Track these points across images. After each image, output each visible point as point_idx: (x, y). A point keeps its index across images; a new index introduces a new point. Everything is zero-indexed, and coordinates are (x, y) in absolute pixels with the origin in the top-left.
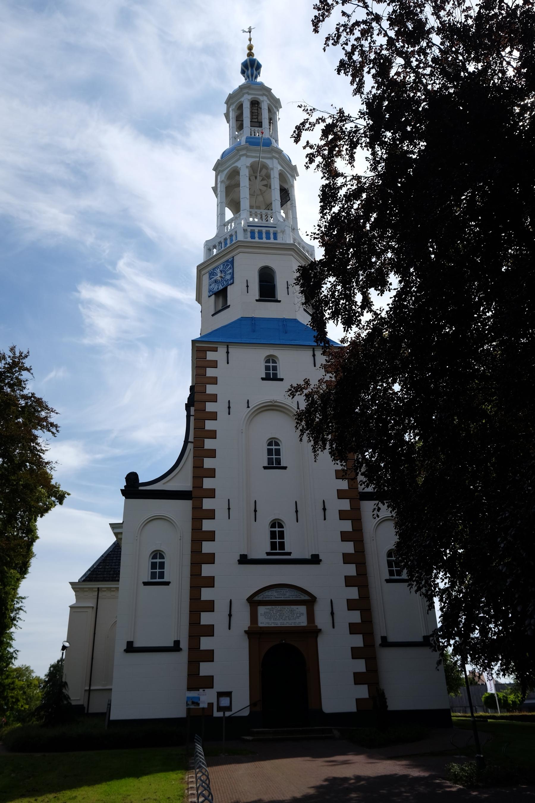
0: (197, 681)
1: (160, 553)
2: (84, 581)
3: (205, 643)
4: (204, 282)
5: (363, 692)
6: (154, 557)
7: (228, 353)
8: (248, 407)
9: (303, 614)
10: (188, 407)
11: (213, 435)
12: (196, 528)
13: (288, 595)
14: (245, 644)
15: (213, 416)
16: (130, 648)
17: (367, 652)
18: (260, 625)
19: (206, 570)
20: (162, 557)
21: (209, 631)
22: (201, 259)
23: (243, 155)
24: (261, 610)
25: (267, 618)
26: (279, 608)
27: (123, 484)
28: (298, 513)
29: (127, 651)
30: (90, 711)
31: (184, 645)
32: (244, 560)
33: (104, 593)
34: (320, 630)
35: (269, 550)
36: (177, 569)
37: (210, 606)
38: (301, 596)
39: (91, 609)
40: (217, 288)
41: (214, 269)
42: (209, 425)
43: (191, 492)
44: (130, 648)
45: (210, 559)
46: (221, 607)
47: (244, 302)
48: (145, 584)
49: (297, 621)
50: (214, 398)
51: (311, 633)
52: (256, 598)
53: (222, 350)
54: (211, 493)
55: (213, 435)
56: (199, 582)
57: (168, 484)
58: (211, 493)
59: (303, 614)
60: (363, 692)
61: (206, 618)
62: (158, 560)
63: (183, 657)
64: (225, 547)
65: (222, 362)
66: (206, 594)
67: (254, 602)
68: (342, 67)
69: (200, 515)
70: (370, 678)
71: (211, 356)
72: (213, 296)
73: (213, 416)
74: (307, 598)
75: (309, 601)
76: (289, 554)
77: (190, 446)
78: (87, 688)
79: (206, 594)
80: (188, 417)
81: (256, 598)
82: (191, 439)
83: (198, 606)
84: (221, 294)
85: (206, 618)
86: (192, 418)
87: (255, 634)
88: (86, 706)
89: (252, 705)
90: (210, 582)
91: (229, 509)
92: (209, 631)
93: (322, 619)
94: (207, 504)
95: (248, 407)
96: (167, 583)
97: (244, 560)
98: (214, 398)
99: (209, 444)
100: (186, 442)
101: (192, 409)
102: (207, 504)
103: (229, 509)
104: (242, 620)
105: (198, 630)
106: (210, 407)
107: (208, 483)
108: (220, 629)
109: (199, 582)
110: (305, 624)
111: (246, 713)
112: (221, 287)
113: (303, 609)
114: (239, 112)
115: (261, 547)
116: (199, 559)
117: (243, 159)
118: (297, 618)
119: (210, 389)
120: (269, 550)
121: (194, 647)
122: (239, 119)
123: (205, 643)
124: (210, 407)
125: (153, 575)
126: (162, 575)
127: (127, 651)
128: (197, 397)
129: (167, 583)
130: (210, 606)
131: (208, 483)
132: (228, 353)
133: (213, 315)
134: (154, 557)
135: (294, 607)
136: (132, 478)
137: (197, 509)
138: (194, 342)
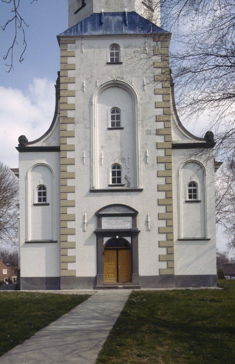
1: (43, 187)
17: (168, 246)
18: (103, 228)
25: (107, 224)
27: (17, 144)
28: (15, 4)
34: (140, 231)
35: (111, 183)
38: (129, 211)
51: (134, 233)
52: (101, 213)
60: (164, 265)
62: (116, 170)
67: (99, 216)
68: (153, 41)
70: (169, 258)
74: (133, 212)
75: (133, 214)
76: (123, 185)
87: (100, 234)
93: (141, 226)
96: (48, 204)
113: (130, 219)
118: (125, 224)
120: (111, 183)
128: (62, 80)
129: (48, 204)
134: (40, 189)
136: (22, 139)
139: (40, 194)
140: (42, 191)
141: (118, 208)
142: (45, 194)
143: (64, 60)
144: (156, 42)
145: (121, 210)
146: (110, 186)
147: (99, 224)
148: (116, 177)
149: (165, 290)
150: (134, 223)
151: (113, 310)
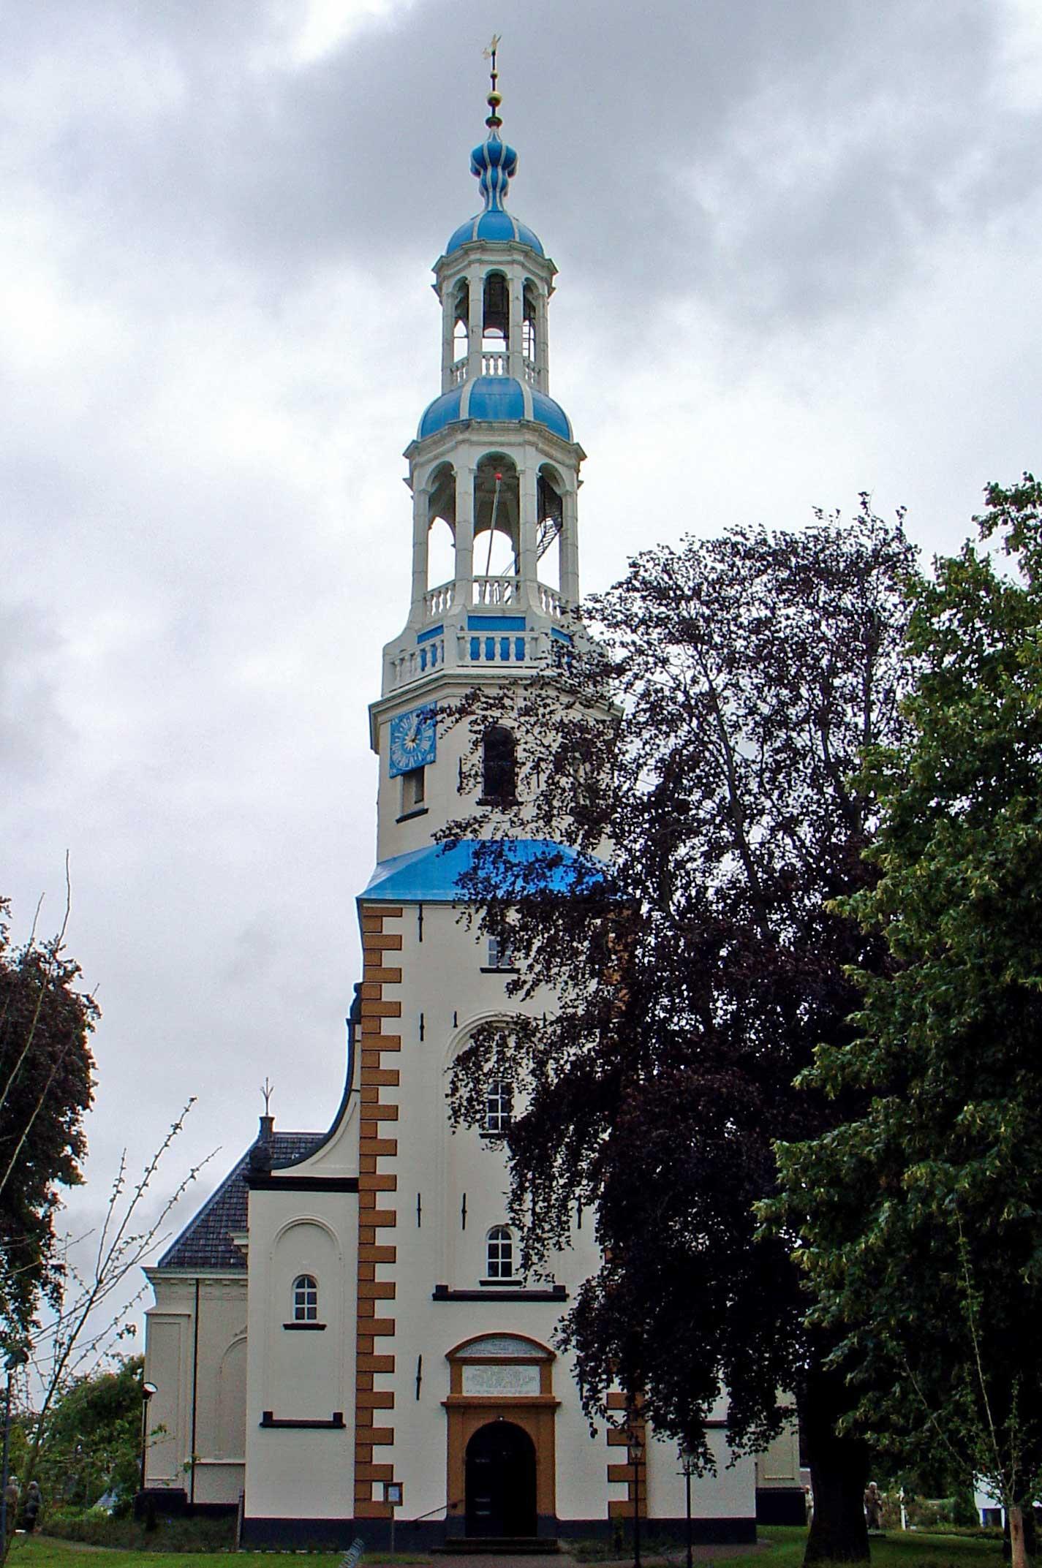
0: (366, 1472)
2: (169, 1263)
3: (381, 1419)
4: (381, 734)
5: (621, 1492)
6: (300, 1285)
7: (421, 919)
8: (456, 1026)
9: (533, 1379)
10: (351, 1023)
11: (393, 1079)
12: (366, 1243)
13: (512, 1350)
14: (442, 1421)
15: (394, 1044)
16: (268, 1421)
19: (382, 1310)
20: (312, 1285)
21: (387, 1401)
22: (362, 872)
23: (463, 441)
24: (468, 1371)
25: (478, 1384)
26: (496, 1368)
29: (263, 1425)
30: (196, 1501)
31: (349, 1420)
32: (442, 1294)
33: (209, 1289)
34: (559, 1404)
36: (337, 1304)
37: (388, 1365)
39: (185, 1319)
40: (408, 763)
41: (401, 719)
42: (387, 1061)
43: (356, 1180)
44: (268, 1421)
45: (389, 1291)
46: (405, 1368)
47: (453, 800)
48: (287, 1327)
49: (525, 1389)
50: (395, 1010)
52: (460, 1355)
53: (411, 914)
54: (390, 1184)
55: (393, 1079)
56: (370, 1328)
57: (320, 1165)
58: (390, 1184)
59: (533, 1379)
60: (621, 1492)
61: (381, 1383)
63: (345, 1440)
64: (409, 1277)
65: (409, 940)
66: (382, 1346)
67: (456, 1360)
69: (371, 1221)
71: (390, 926)
72: (399, 778)
73: (394, 1044)
77: (355, 1098)
78: (188, 1460)
79: (382, 1346)
80: (352, 1042)
81: (458, 1355)
82: (356, 1085)
83: (370, 1365)
84: (415, 775)
85: (381, 1383)
86: (358, 1047)
87: (456, 1408)
88: (188, 1490)
89: (452, 1506)
90: (388, 1328)
91: (419, 1210)
92: (387, 1401)
94: (384, 1201)
95: (456, 1026)
96: (322, 1327)
97: (442, 1294)
98: (395, 1010)
99: (386, 1096)
100: (349, 1090)
101: (358, 1028)
102: (384, 1201)
103: (419, 1210)
104: (438, 1387)
105: (369, 1401)
106: (389, 1027)
107: (384, 1166)
108: (403, 1395)
109: (370, 1328)
110: (537, 1394)
111: (441, 1516)
112: (412, 765)
113: (534, 1371)
114: (460, 295)
115: (473, 1273)
116: (370, 1291)
117: (464, 449)
119: (389, 993)
121: (364, 1424)
122: (461, 311)
123: (381, 1419)
124: (389, 1027)
125: (300, 1314)
126: (312, 1314)
127: (263, 1425)
128: (366, 1009)
129: (322, 1327)
130: (388, 1365)
131: (384, 1166)
132: (421, 919)
133: (398, 821)
134: (300, 1285)
135: (521, 1368)
137: (367, 1208)
138: (360, 901)
139: (299, 1298)
140: (306, 1290)
141: (504, 1343)
142: (313, 1298)
143: (374, 958)
144: (465, 333)
145: (511, 1348)
146: (483, 1283)
147: (456, 1383)
148: (500, 1260)
149: (487, 1422)
150: (546, 1383)
151: (105, 1496)
